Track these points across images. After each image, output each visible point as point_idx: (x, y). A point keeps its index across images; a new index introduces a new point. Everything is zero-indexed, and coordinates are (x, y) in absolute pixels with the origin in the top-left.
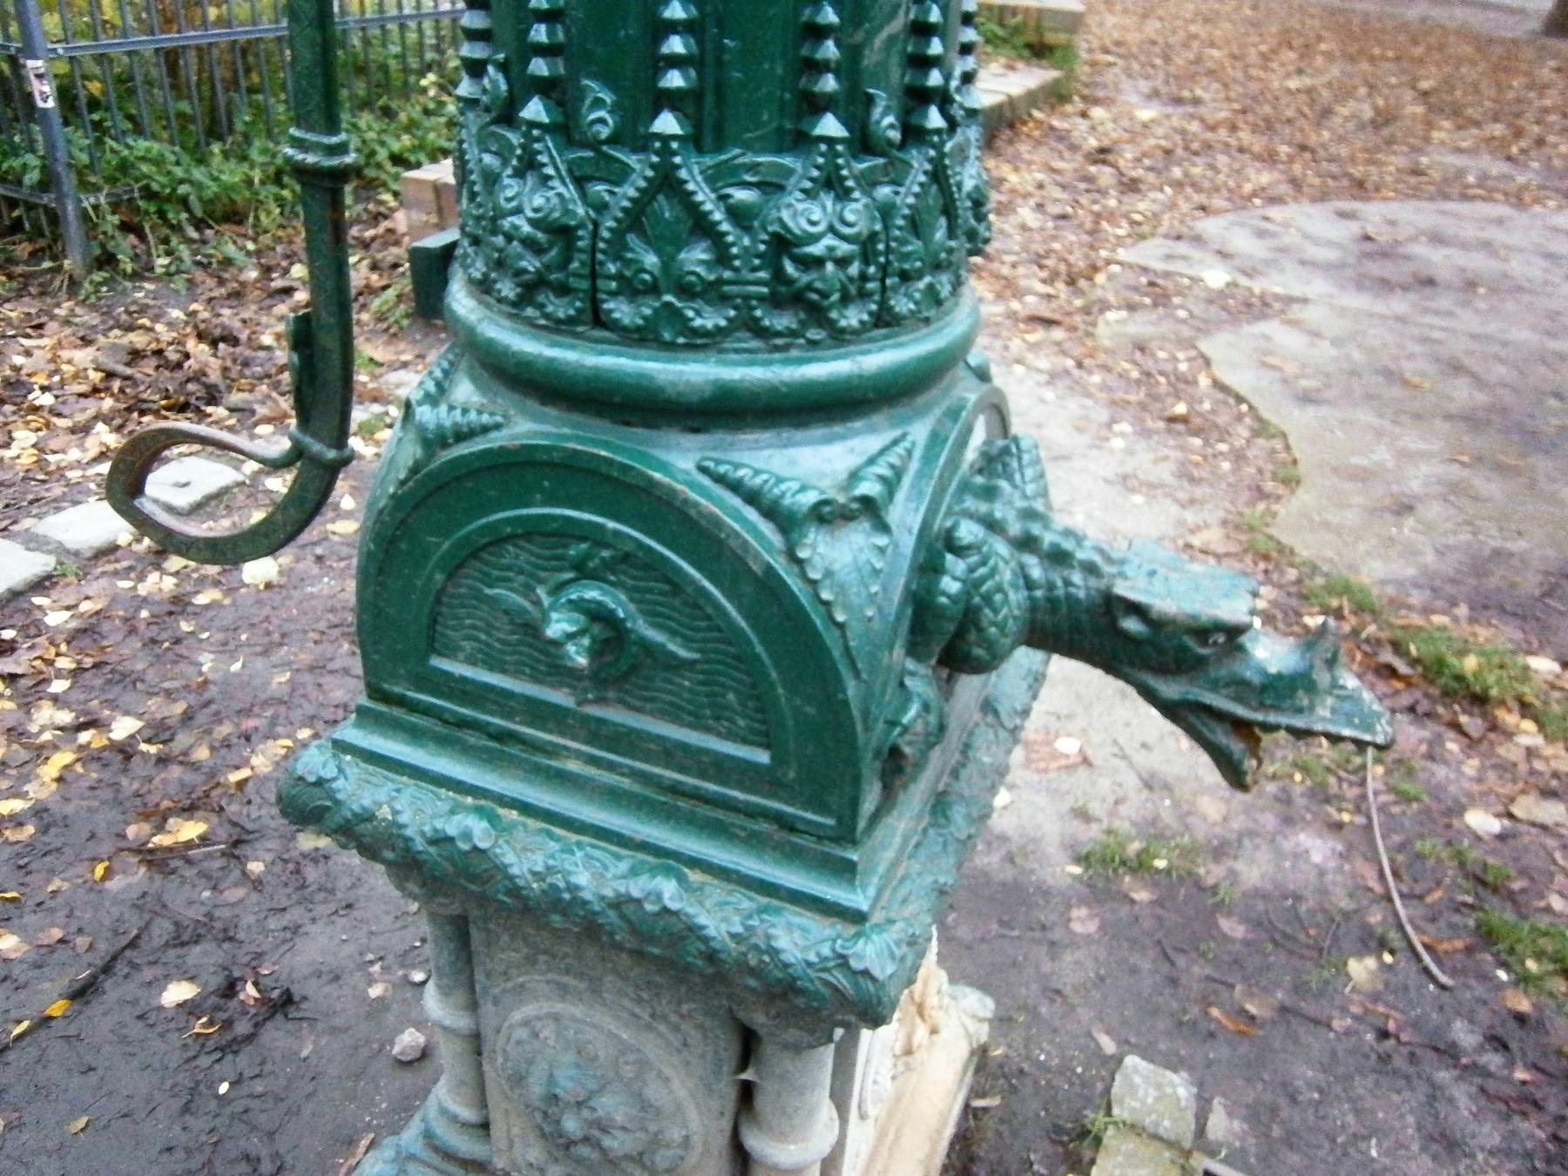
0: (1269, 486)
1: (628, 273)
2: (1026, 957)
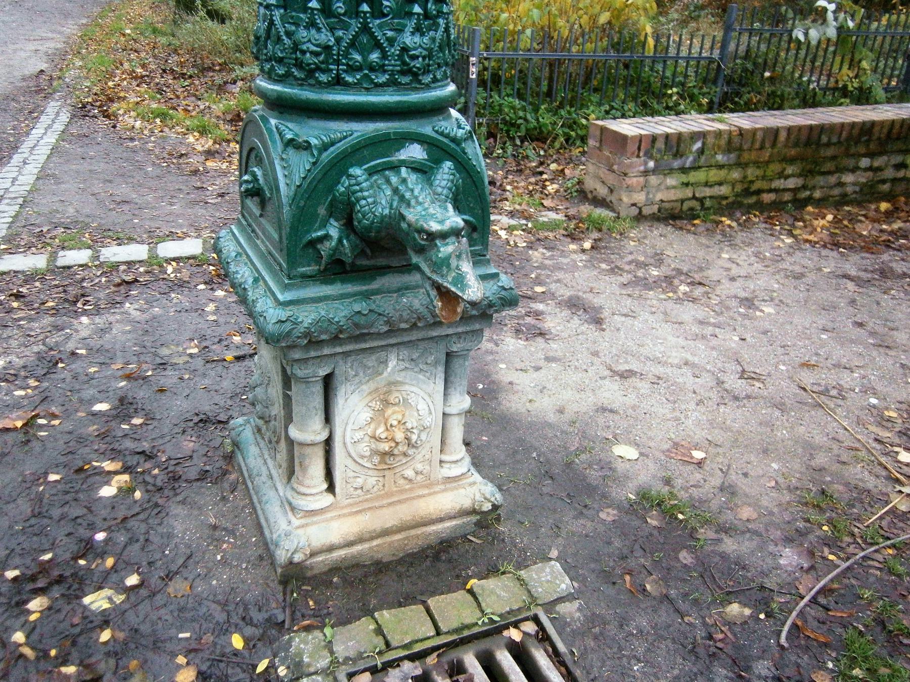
1: (350, 63)
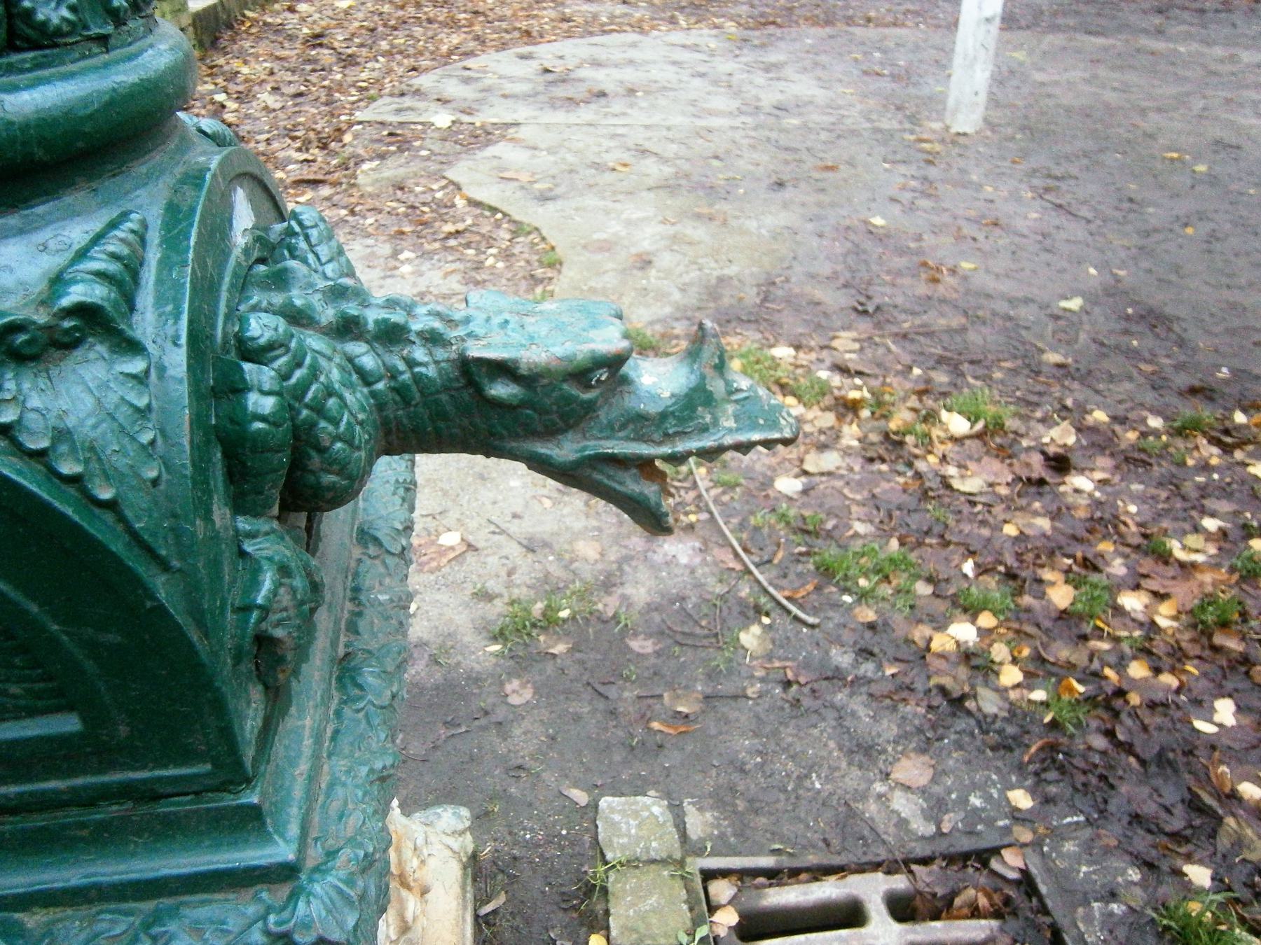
0: (539, 272)
2: (480, 749)
